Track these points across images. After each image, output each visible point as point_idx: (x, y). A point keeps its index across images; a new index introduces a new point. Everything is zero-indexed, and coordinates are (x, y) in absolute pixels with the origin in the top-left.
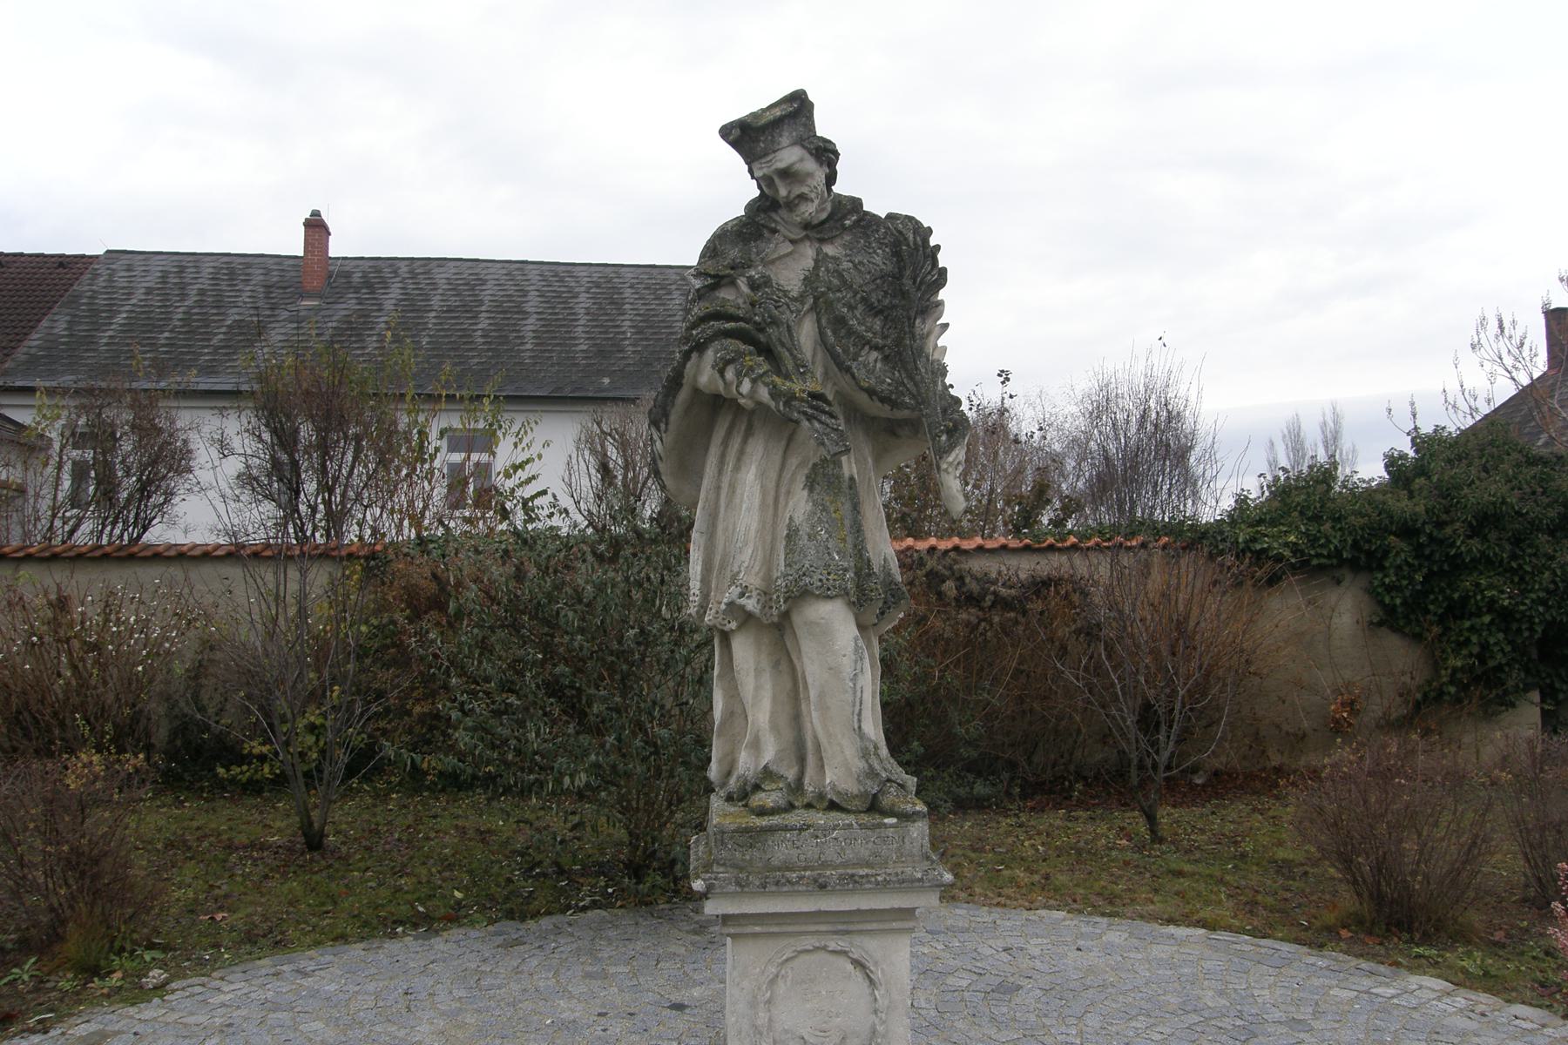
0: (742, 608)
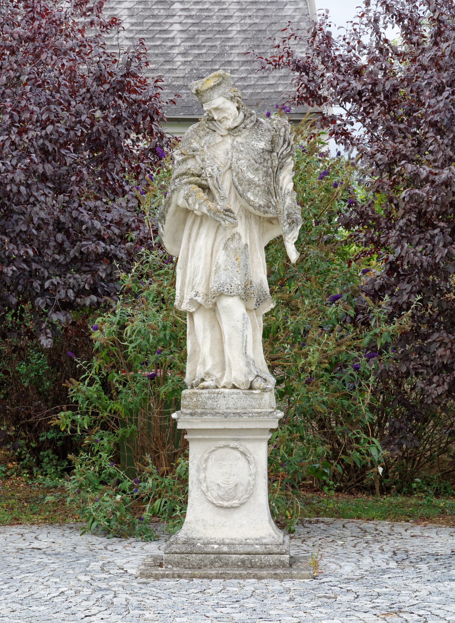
0: (196, 301)
